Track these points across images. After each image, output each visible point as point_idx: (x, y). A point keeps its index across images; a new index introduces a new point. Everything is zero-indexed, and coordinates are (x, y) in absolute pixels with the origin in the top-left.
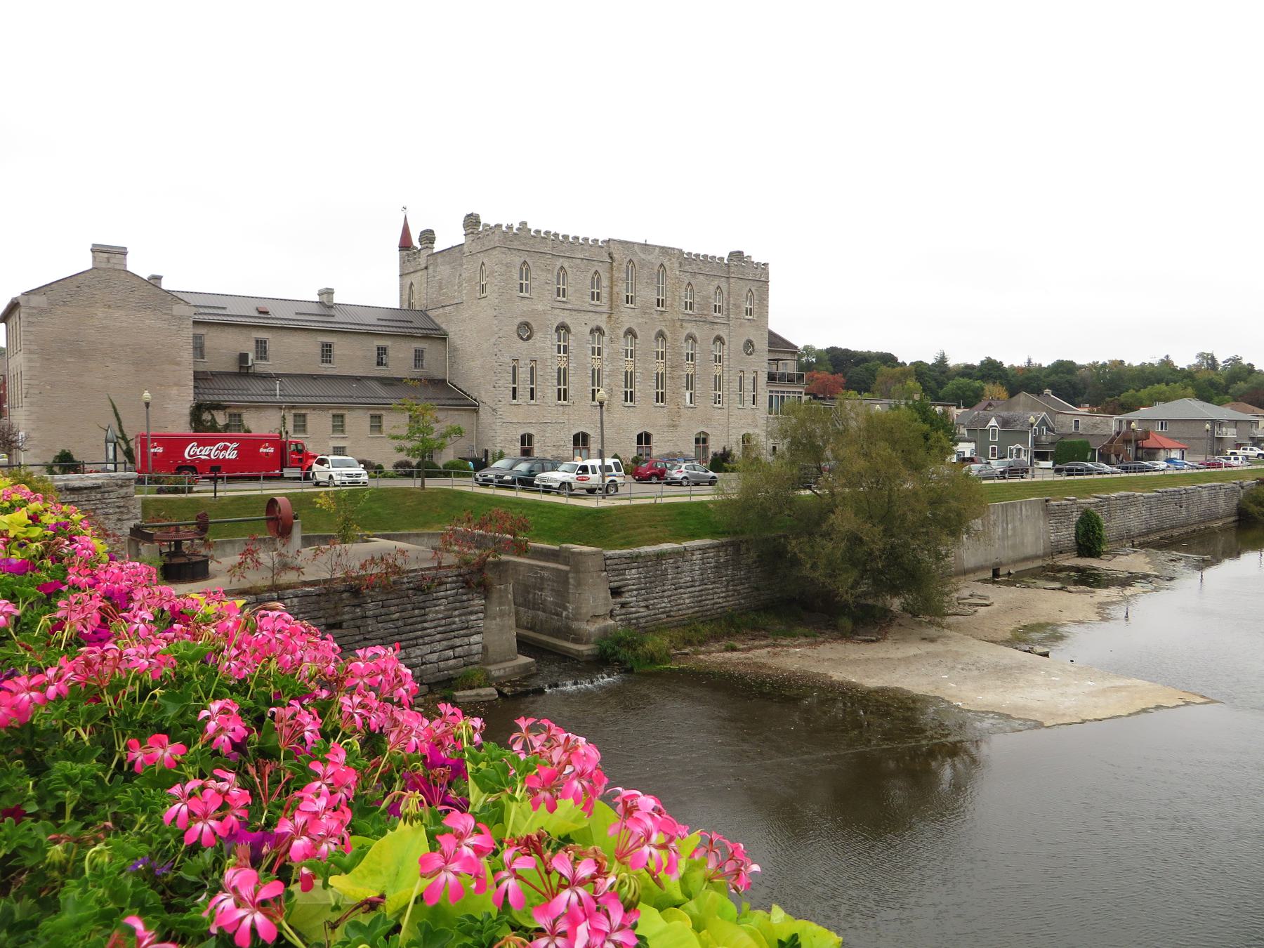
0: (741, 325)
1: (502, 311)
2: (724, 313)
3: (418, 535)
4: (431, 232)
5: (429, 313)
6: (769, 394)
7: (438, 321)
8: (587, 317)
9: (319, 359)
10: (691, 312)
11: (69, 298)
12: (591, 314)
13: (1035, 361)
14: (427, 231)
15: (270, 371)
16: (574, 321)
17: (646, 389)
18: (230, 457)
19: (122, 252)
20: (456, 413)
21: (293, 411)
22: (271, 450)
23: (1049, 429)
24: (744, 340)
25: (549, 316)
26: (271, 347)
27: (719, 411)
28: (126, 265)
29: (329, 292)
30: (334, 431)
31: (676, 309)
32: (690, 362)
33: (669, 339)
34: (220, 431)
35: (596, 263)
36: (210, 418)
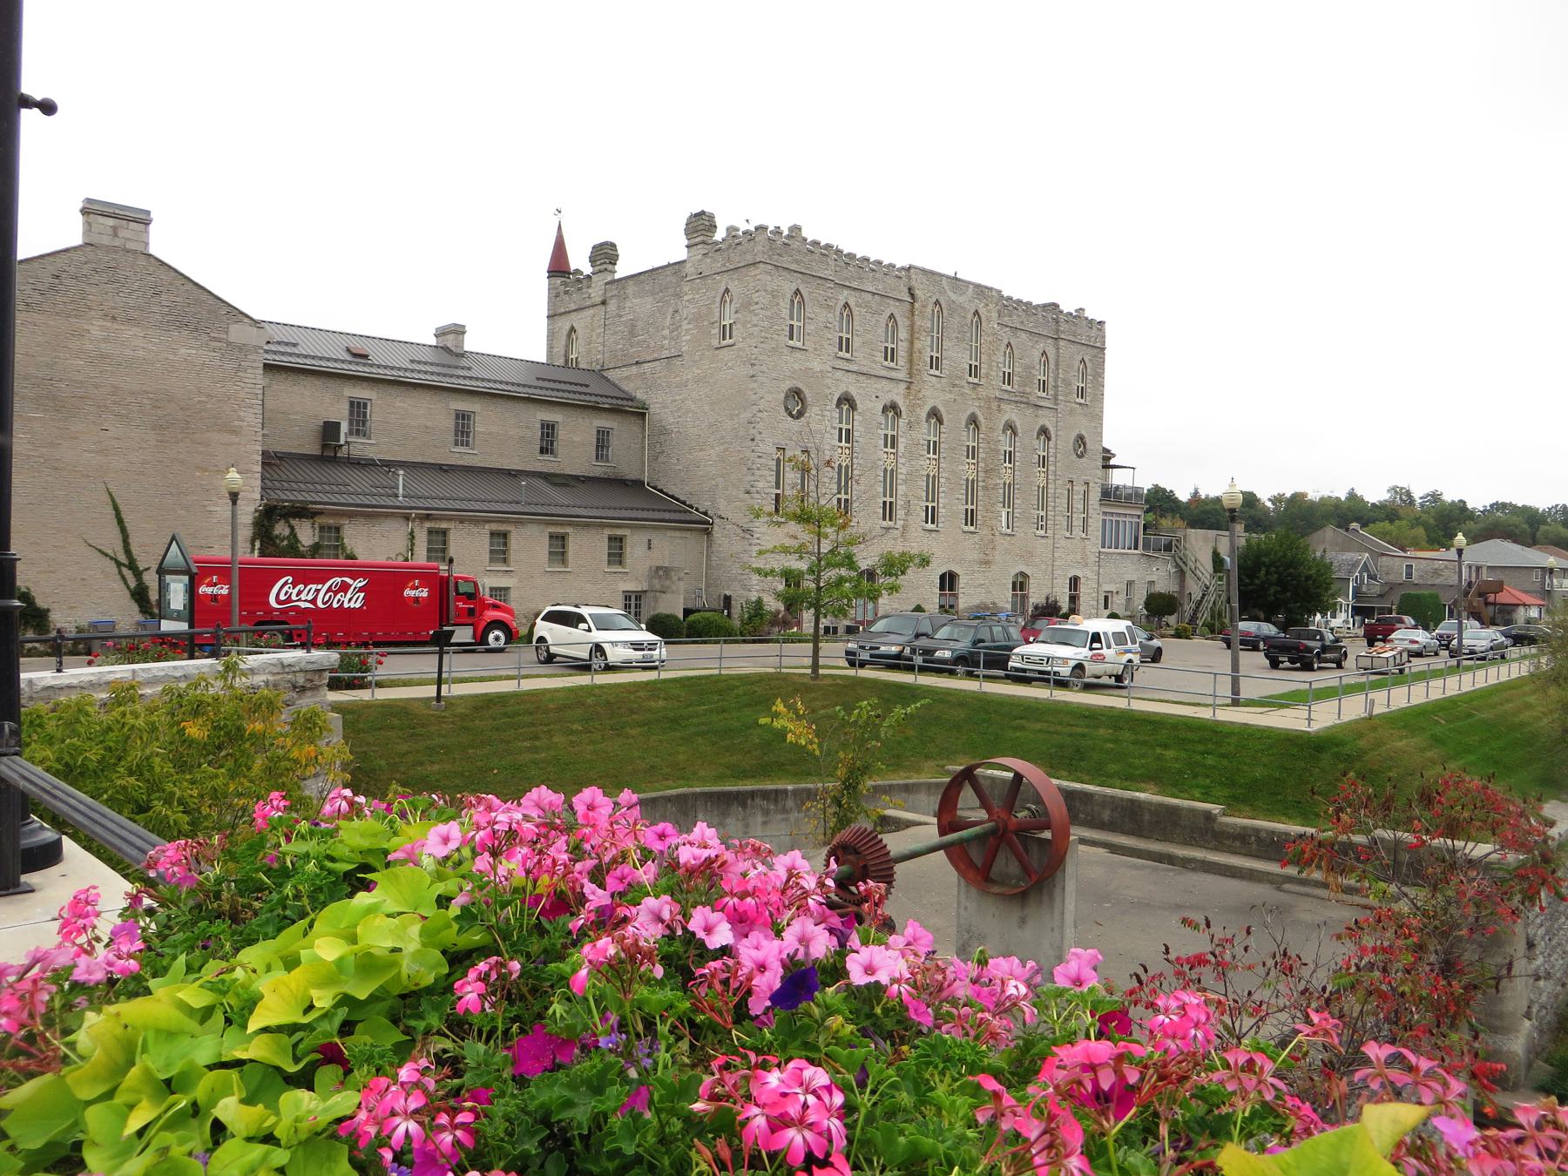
0: (1072, 411)
1: (764, 368)
2: (1051, 392)
3: (907, 788)
4: (613, 246)
5: (610, 375)
6: (1102, 517)
7: (628, 387)
8: (878, 386)
9: (451, 438)
10: (1009, 388)
11: (37, 297)
12: (884, 382)
13: (1203, 493)
14: (606, 243)
15: (370, 456)
16: (861, 391)
17: (951, 504)
18: (352, 605)
19: (142, 219)
20: (678, 534)
21: (428, 525)
22: (424, 593)
23: (1372, 577)
24: (1073, 436)
25: (829, 381)
26: (375, 414)
27: (1043, 541)
28: (147, 244)
29: (458, 331)
30: (492, 560)
31: (993, 385)
32: (1007, 464)
33: (983, 428)
34: (303, 557)
35: (891, 302)
36: (287, 532)
